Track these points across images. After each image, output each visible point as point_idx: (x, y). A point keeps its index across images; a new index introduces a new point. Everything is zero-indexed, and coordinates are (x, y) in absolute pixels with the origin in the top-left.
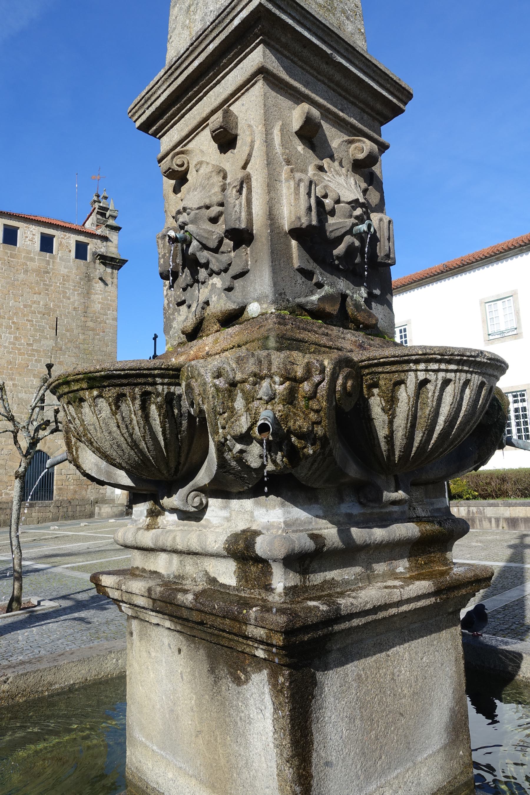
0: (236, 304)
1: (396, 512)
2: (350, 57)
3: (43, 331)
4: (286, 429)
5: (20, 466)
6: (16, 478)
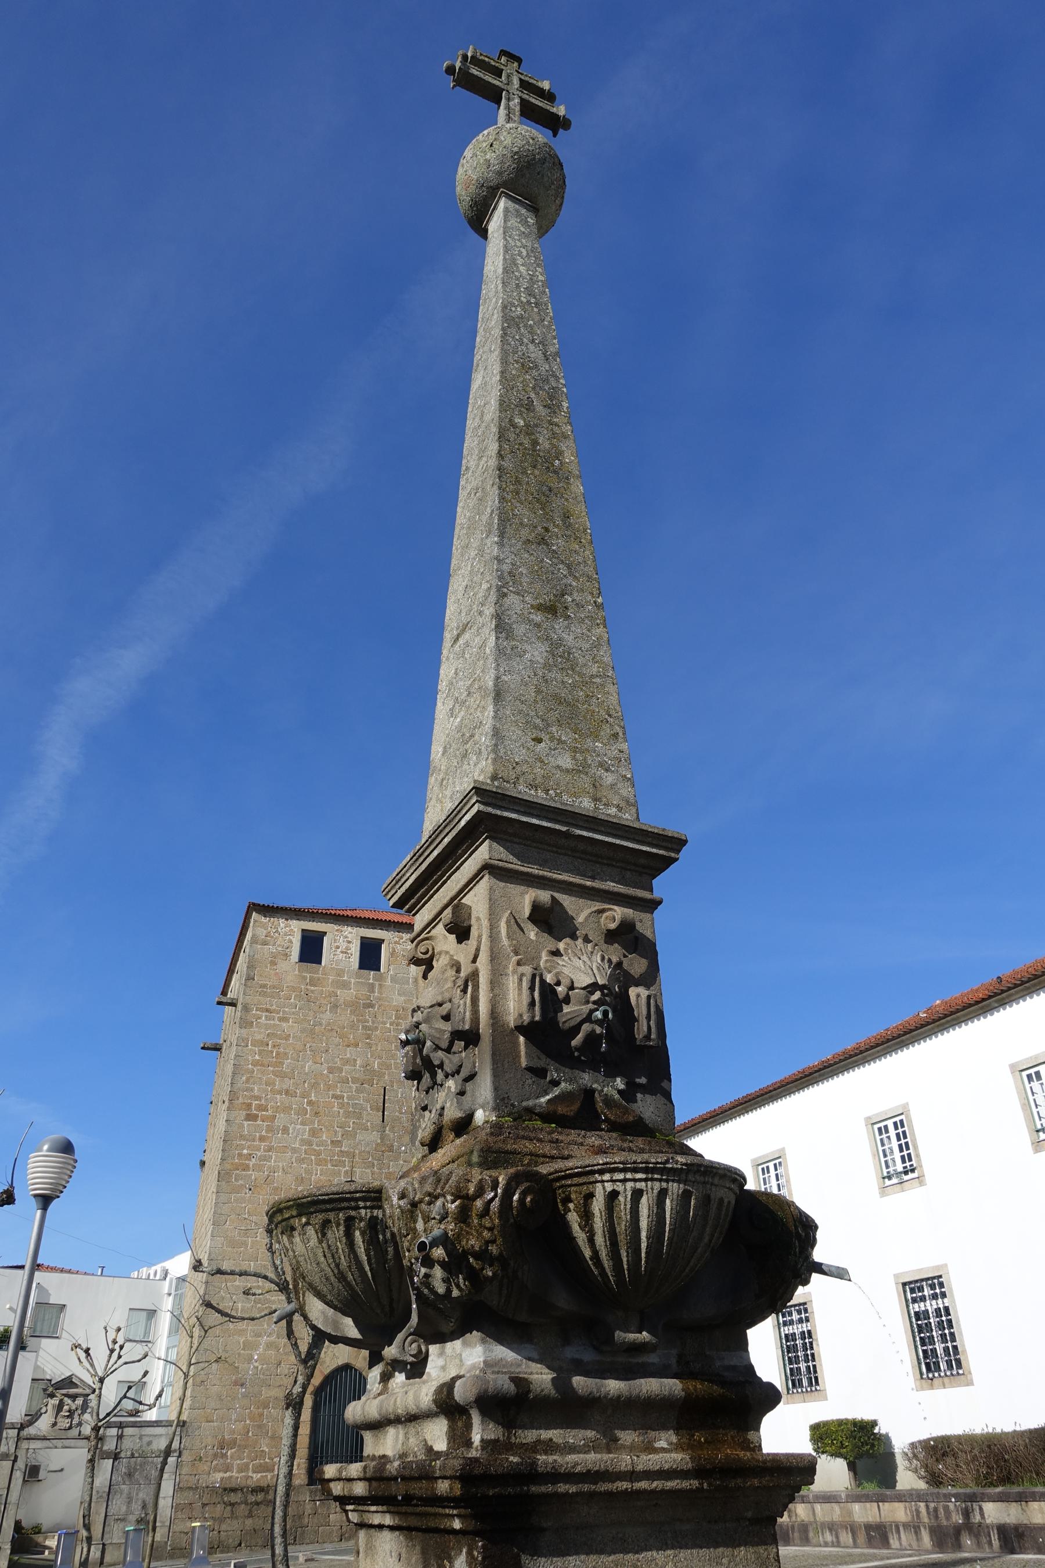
0: (462, 1112)
1: (654, 1364)
2: (592, 826)
3: (359, 1116)
4: (461, 1249)
5: (295, 1382)
6: (287, 1408)
